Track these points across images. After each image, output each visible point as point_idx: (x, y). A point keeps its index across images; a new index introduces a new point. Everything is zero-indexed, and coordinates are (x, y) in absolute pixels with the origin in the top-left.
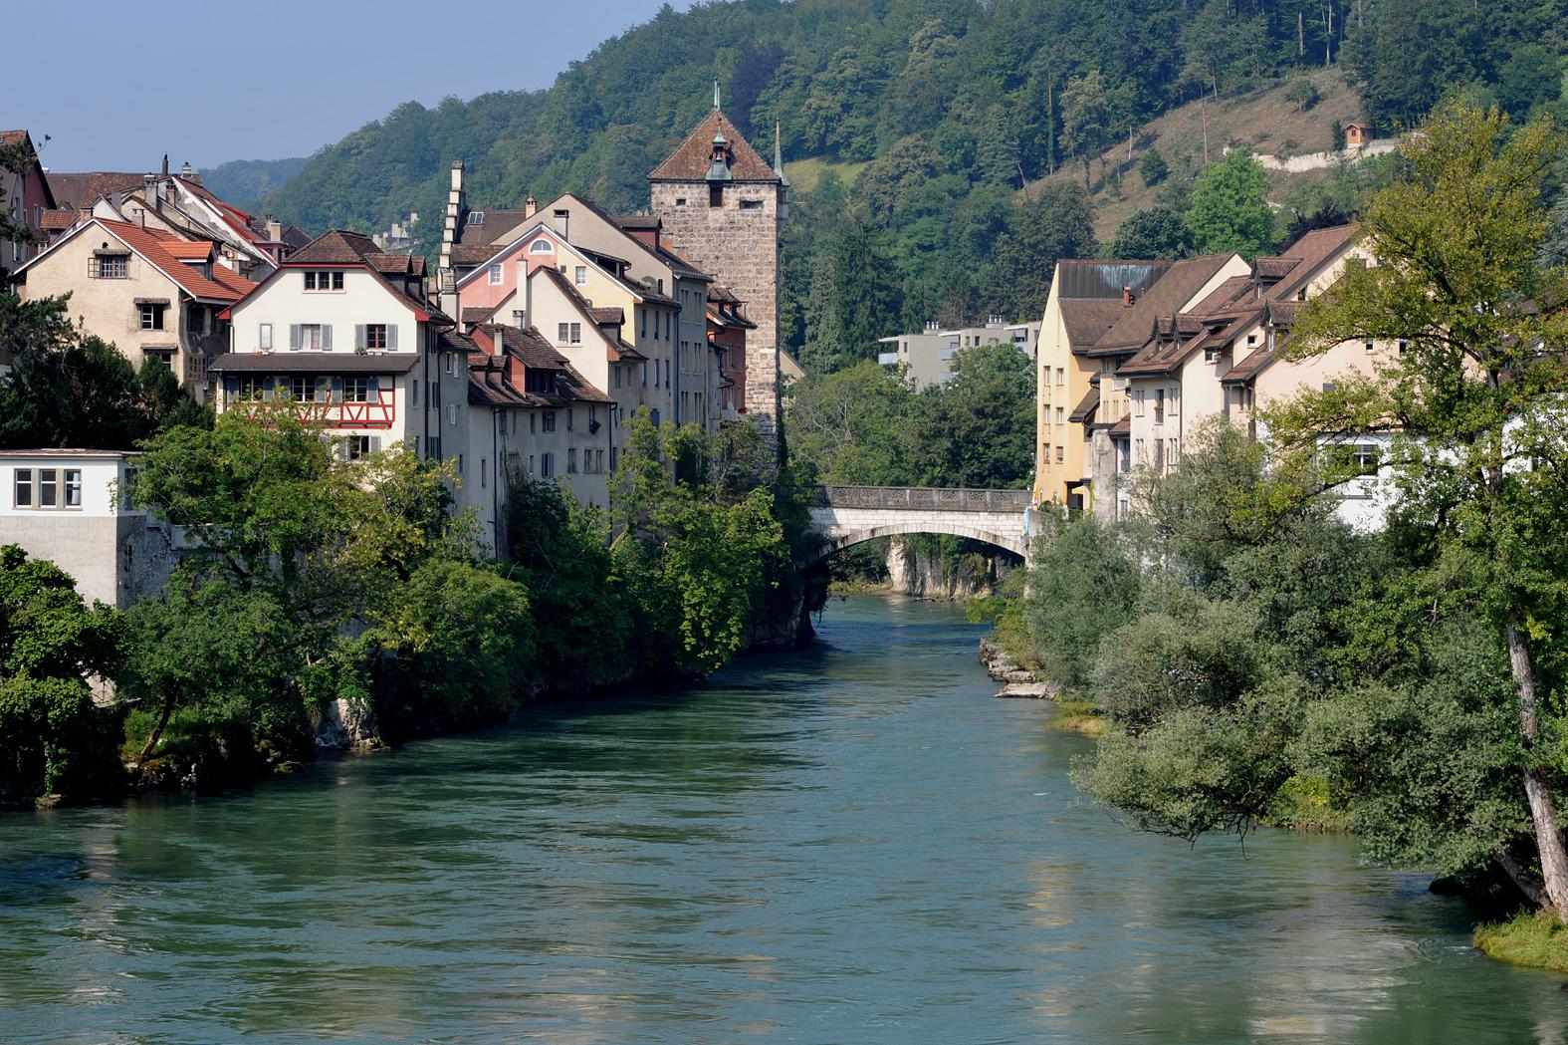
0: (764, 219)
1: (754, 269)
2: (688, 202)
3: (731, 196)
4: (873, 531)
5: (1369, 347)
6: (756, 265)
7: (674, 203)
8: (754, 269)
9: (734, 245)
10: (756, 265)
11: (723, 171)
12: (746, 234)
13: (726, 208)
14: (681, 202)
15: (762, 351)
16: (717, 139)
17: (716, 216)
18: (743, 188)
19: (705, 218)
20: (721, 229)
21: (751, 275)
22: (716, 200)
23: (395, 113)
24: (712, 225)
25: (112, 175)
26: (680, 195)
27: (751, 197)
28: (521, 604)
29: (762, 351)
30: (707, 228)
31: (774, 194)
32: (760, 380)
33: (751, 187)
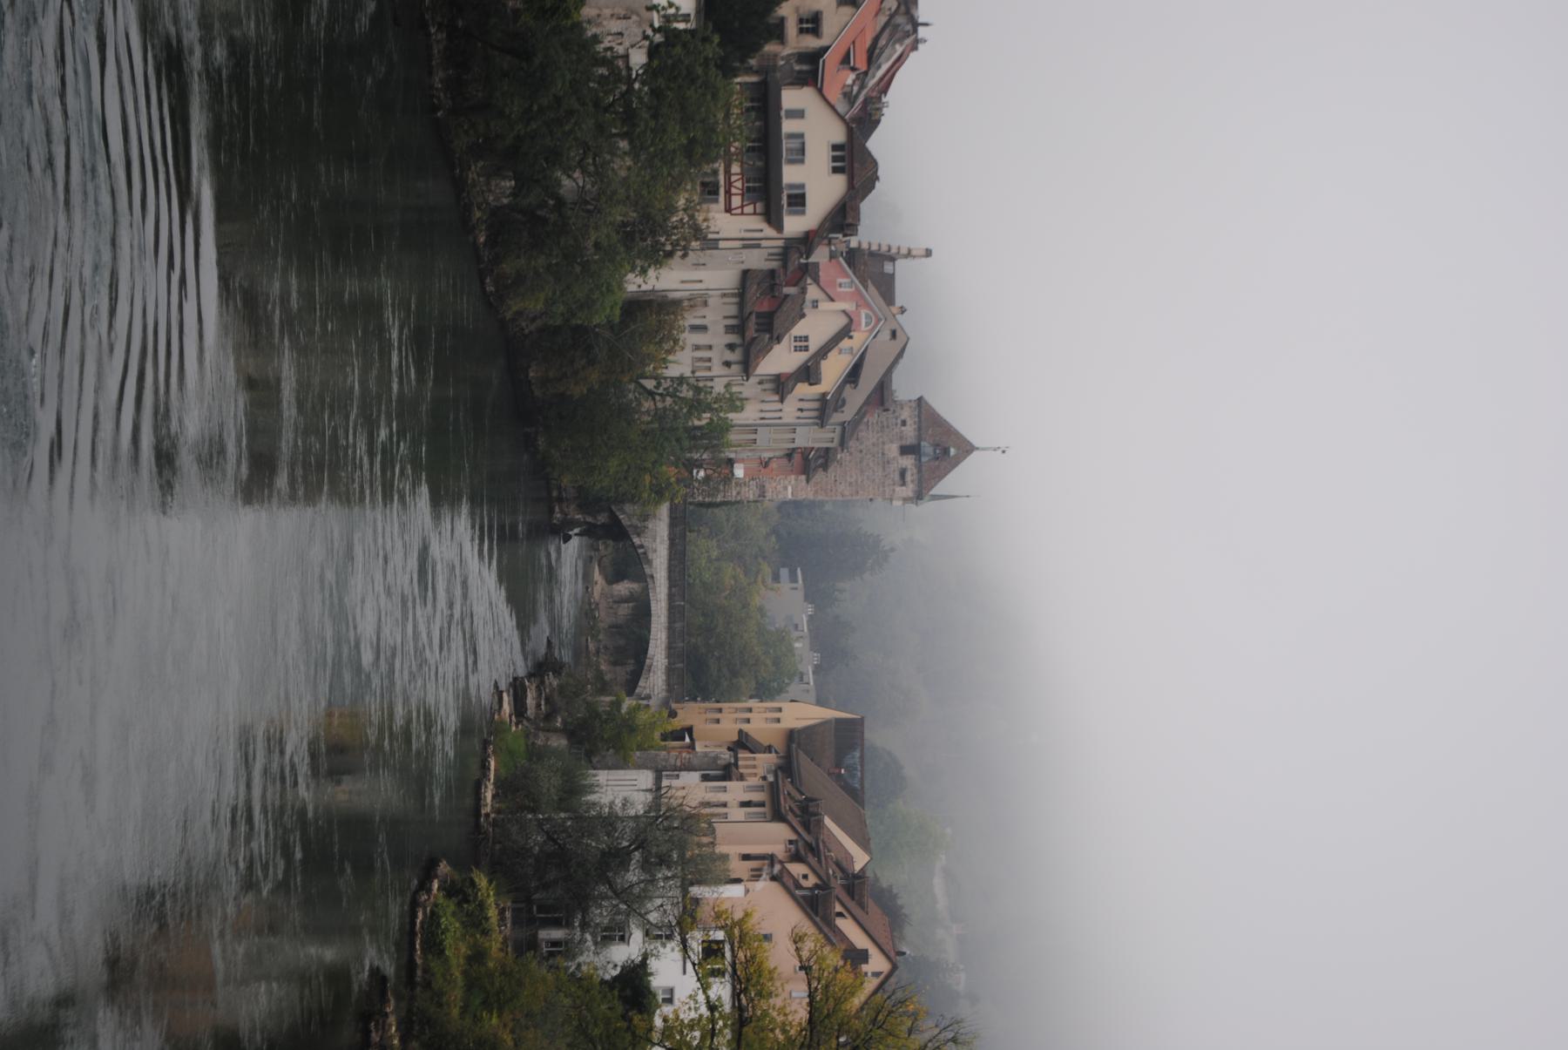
3: (908, 462)
14: (904, 423)
17: (893, 450)
22: (905, 450)
26: (909, 422)
27: (908, 478)
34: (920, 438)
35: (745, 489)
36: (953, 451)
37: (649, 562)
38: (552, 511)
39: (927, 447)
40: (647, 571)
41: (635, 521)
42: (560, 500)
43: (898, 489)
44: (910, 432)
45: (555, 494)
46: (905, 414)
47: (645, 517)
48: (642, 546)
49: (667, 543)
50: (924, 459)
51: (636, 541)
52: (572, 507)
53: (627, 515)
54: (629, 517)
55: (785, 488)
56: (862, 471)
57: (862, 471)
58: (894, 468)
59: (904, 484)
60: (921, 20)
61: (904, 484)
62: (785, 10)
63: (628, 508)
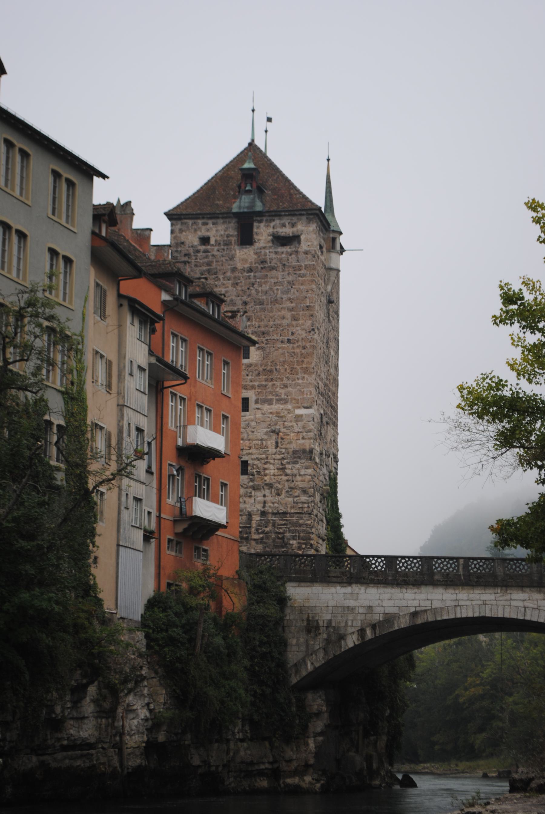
0: (301, 256)
1: (288, 315)
2: (212, 241)
3: (263, 233)
4: (415, 614)
5: (68, 320)
6: (291, 310)
7: (196, 242)
8: (288, 315)
9: (266, 287)
10: (291, 310)
11: (253, 202)
12: (280, 274)
13: (257, 245)
14: (205, 240)
15: (299, 412)
16: (246, 165)
17: (244, 256)
18: (277, 222)
19: (232, 258)
20: (250, 270)
21: (285, 322)
22: (246, 238)
23: (87, 407)
24: (239, 266)
25: (337, 386)
26: (203, 232)
27: (288, 231)
28: (24, 402)
29: (299, 412)
30: (234, 270)
31: (313, 227)
32: (293, 446)
33: (286, 220)
34: (227, 215)
35: (299, 482)
36: (248, 165)
37: (389, 619)
38: (296, 791)
39: (241, 204)
40: (404, 623)
41: (318, 643)
42: (275, 774)
43: (304, 246)
44: (217, 231)
45: (264, 783)
46: (191, 239)
47: (312, 627)
48: (362, 632)
49: (356, 588)
50: (259, 207)
51: (351, 641)
52: (289, 753)
53: (304, 656)
54: (310, 653)
55: (298, 418)
56: (276, 301)
57: (276, 301)
58: (272, 254)
59: (294, 239)
60: (98, 533)
61: (294, 239)
62: (543, 795)
63: (293, 655)
